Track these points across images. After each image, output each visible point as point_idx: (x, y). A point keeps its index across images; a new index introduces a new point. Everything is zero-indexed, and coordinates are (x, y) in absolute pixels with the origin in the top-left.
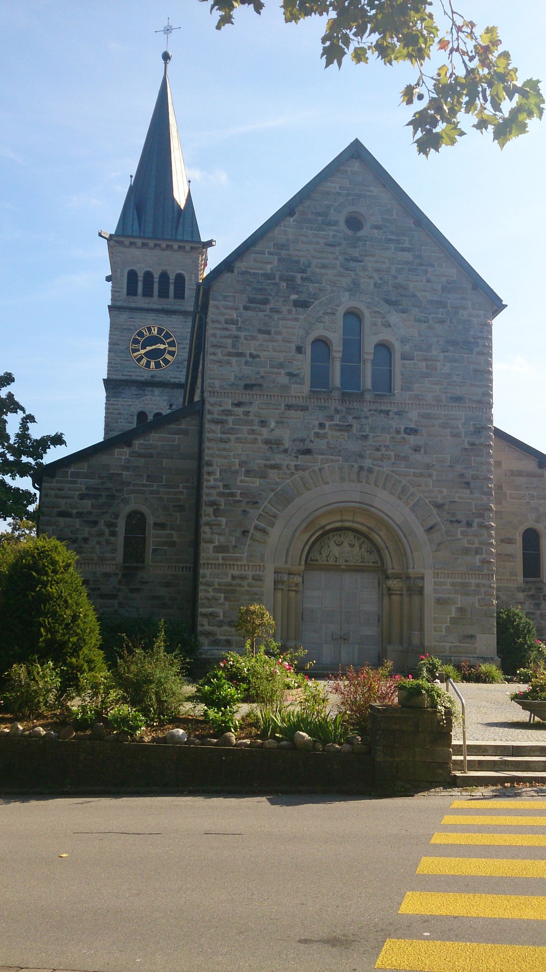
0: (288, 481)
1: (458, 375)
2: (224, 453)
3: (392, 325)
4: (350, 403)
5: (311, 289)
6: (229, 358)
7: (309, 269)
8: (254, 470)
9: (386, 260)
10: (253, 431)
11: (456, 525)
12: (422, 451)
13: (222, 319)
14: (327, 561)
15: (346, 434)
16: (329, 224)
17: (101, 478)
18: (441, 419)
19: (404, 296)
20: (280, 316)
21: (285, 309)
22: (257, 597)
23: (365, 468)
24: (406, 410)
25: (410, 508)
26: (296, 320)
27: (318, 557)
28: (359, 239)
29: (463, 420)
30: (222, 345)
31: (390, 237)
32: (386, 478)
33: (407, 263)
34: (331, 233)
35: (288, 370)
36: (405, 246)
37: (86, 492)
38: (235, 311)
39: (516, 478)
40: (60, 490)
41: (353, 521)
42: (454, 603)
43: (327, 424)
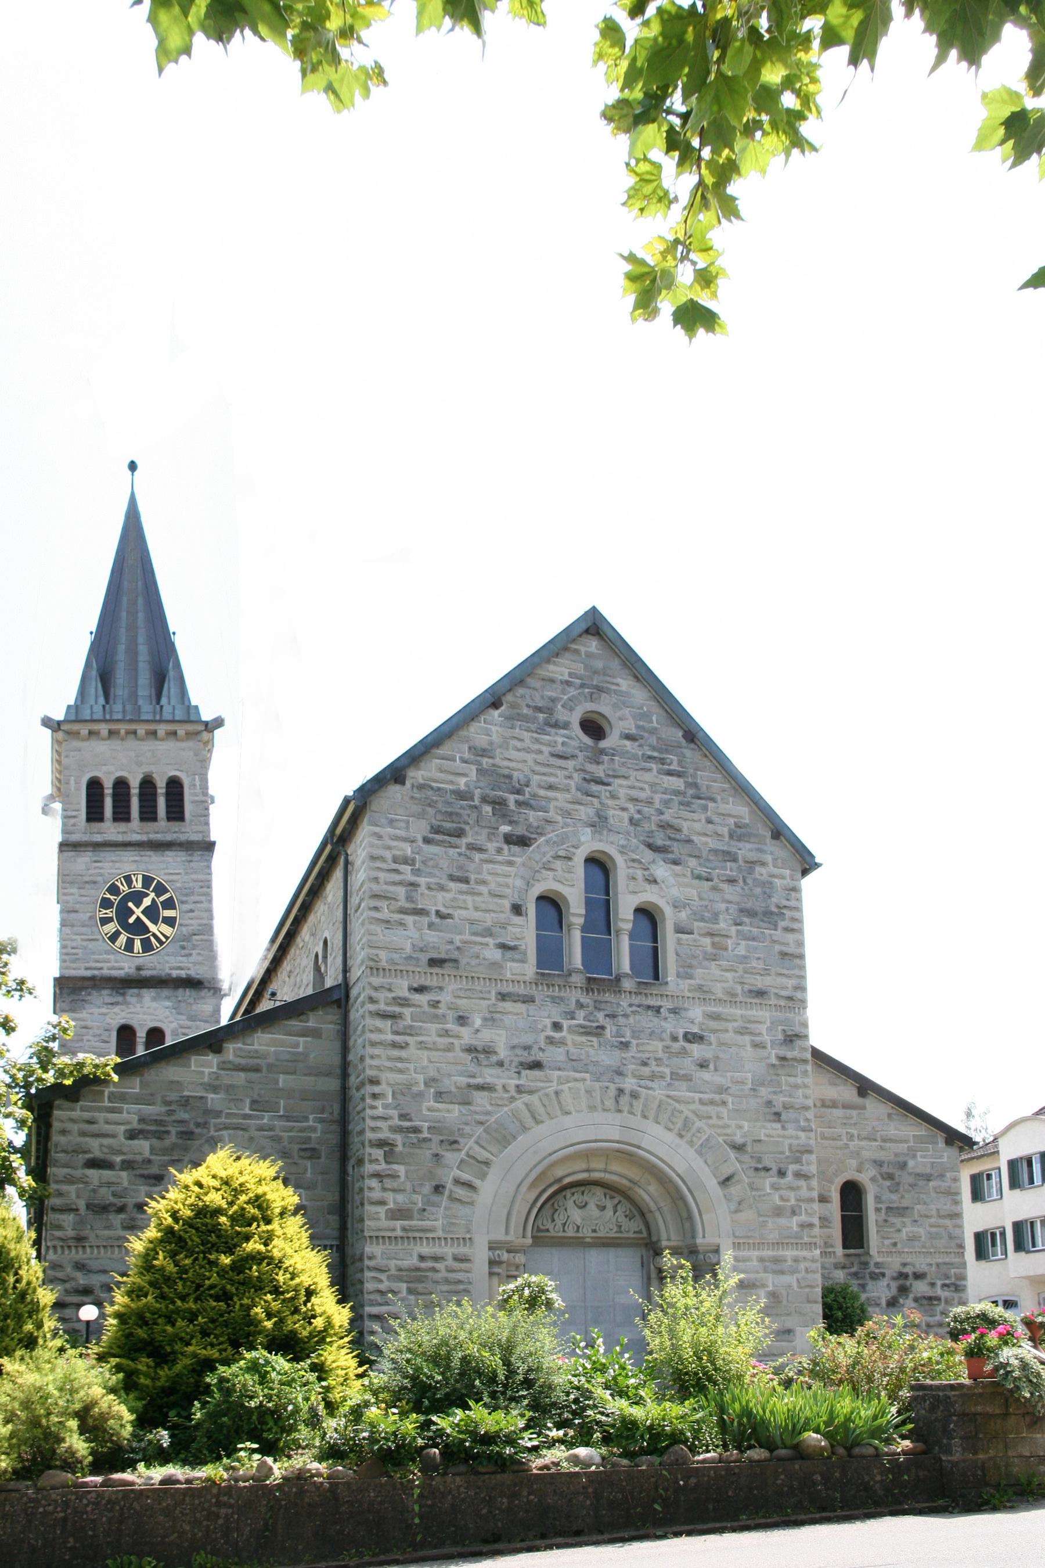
0: (506, 1109)
1: (759, 959)
2: (399, 1065)
3: (659, 880)
4: (599, 993)
5: (531, 820)
6: (402, 916)
7: (527, 790)
8: (450, 1092)
9: (646, 786)
10: (447, 1031)
11: (763, 1173)
12: (712, 1066)
13: (388, 855)
14: (564, 1231)
15: (594, 1039)
16: (556, 725)
17: (167, 1103)
18: (736, 1020)
19: (675, 840)
20: (484, 856)
21: (491, 846)
22: (461, 1287)
23: (627, 1092)
24: (686, 1006)
25: (696, 1151)
26: (510, 863)
27: (549, 1225)
28: (602, 752)
29: (768, 1024)
30: (389, 895)
31: (649, 753)
32: (659, 1106)
33: (677, 793)
34: (560, 740)
35: (500, 940)
36: (672, 767)
37: (139, 1127)
38: (408, 844)
39: (830, 1110)
40: (90, 1122)
41: (605, 1171)
42: (764, 1286)
43: (566, 1024)
